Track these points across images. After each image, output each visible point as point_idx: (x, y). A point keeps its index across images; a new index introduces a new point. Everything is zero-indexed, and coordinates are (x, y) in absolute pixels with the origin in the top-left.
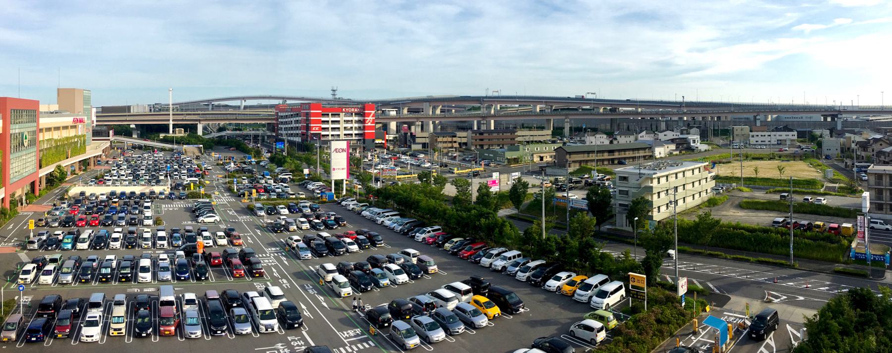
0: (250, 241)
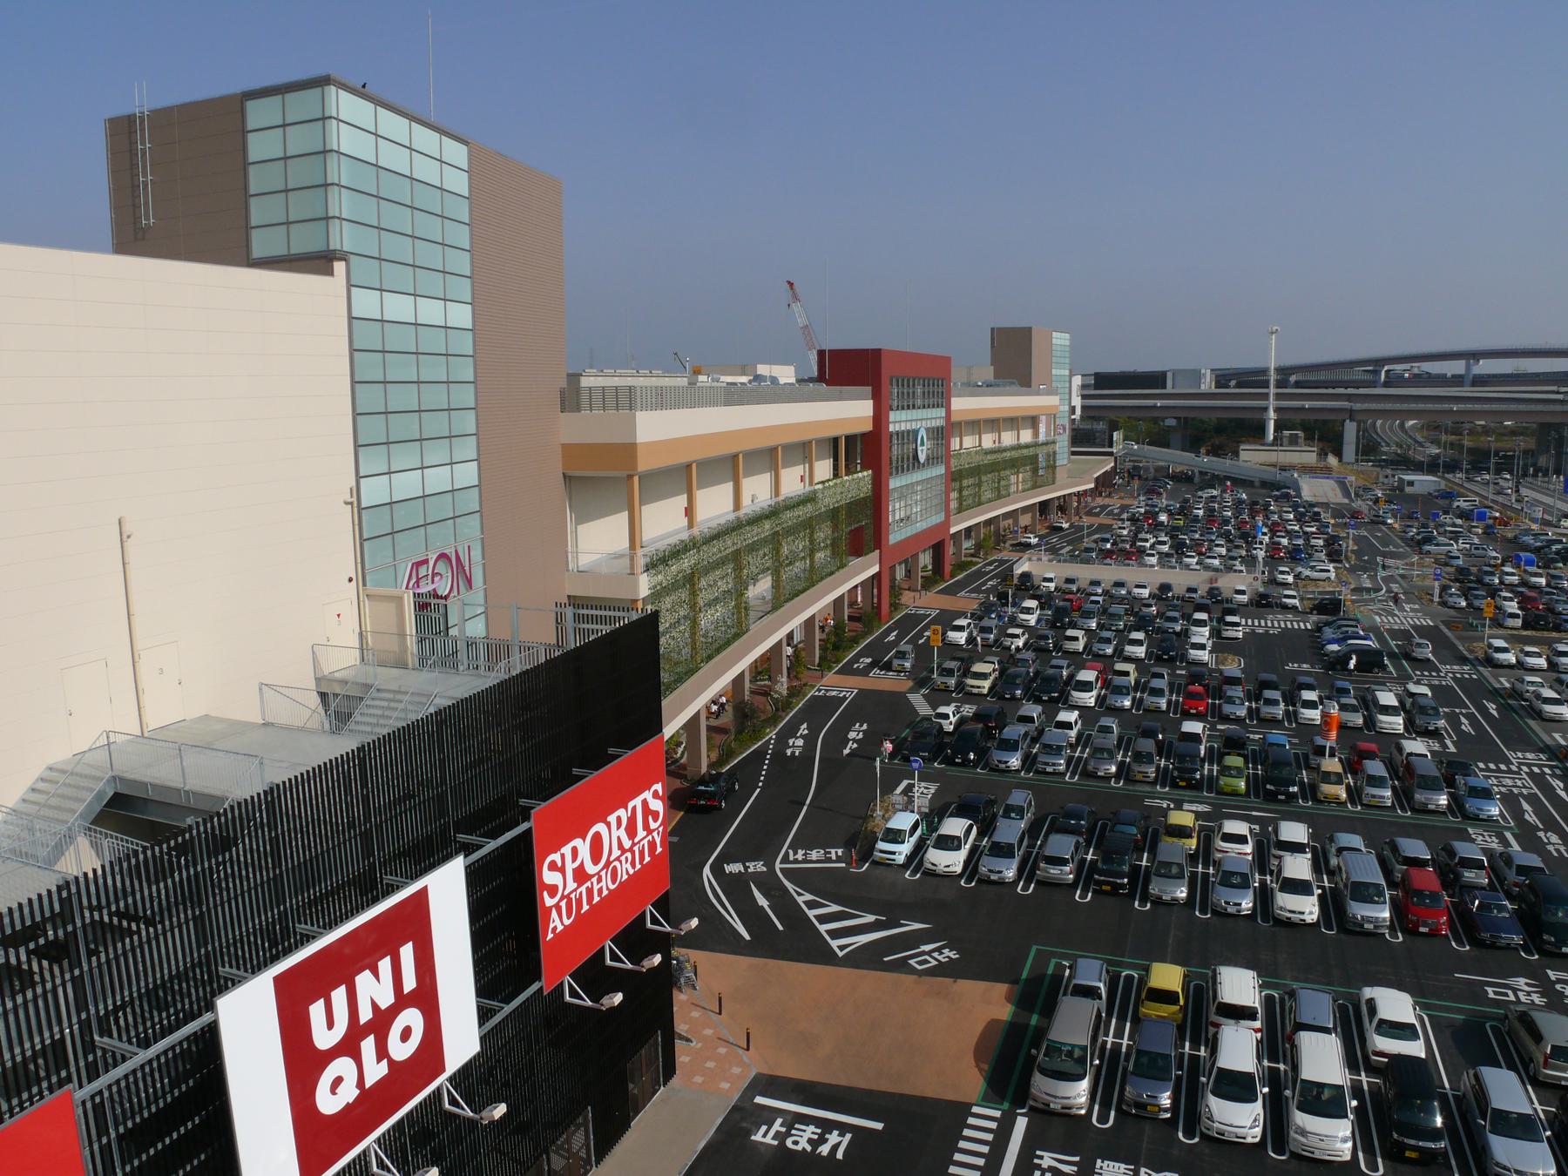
0: (1466, 726)
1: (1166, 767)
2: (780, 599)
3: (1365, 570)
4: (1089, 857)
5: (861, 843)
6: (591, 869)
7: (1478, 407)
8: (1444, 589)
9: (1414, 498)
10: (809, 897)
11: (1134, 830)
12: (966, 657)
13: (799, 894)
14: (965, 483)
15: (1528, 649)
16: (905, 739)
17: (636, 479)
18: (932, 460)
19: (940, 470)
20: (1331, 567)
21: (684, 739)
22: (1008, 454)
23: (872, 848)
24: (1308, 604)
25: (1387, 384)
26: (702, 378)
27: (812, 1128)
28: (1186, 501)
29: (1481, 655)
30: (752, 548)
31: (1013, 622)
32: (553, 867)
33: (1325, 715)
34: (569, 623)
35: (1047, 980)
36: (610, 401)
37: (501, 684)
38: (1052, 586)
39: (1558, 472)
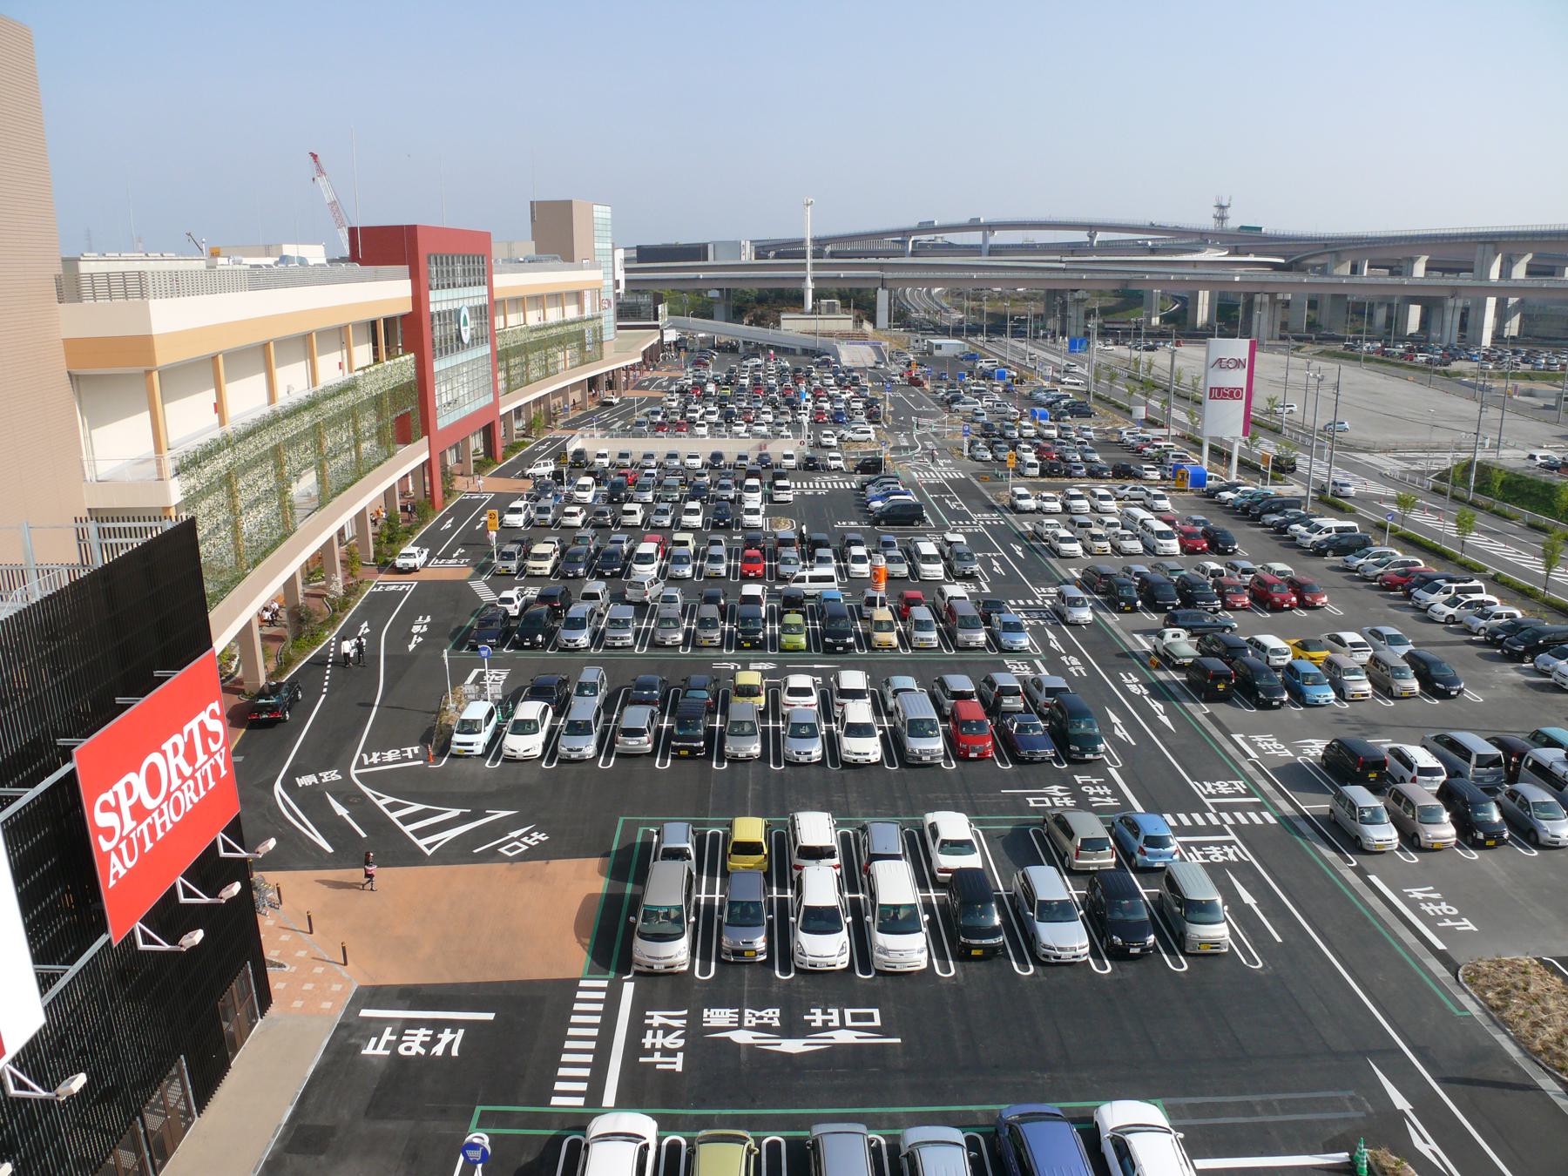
0: (997, 569)
1: (730, 632)
2: (325, 497)
3: (901, 429)
4: (665, 725)
5: (437, 739)
6: (149, 803)
7: (995, 275)
8: (972, 443)
9: (941, 361)
10: (389, 800)
11: (705, 694)
12: (524, 542)
13: (379, 798)
14: (512, 362)
15: (1045, 494)
16: (471, 628)
17: (155, 375)
18: (476, 340)
19: (486, 350)
20: (871, 428)
21: (236, 651)
22: (554, 331)
23: (448, 742)
24: (853, 465)
25: (913, 254)
26: (221, 260)
27: (423, 1031)
28: (732, 371)
29: (1006, 502)
30: (292, 443)
31: (570, 500)
32: (106, 807)
33: (874, 568)
34: (93, 539)
35: (637, 850)
36: (117, 289)
37: (19, 615)
38: (606, 462)
39: (1063, 334)
